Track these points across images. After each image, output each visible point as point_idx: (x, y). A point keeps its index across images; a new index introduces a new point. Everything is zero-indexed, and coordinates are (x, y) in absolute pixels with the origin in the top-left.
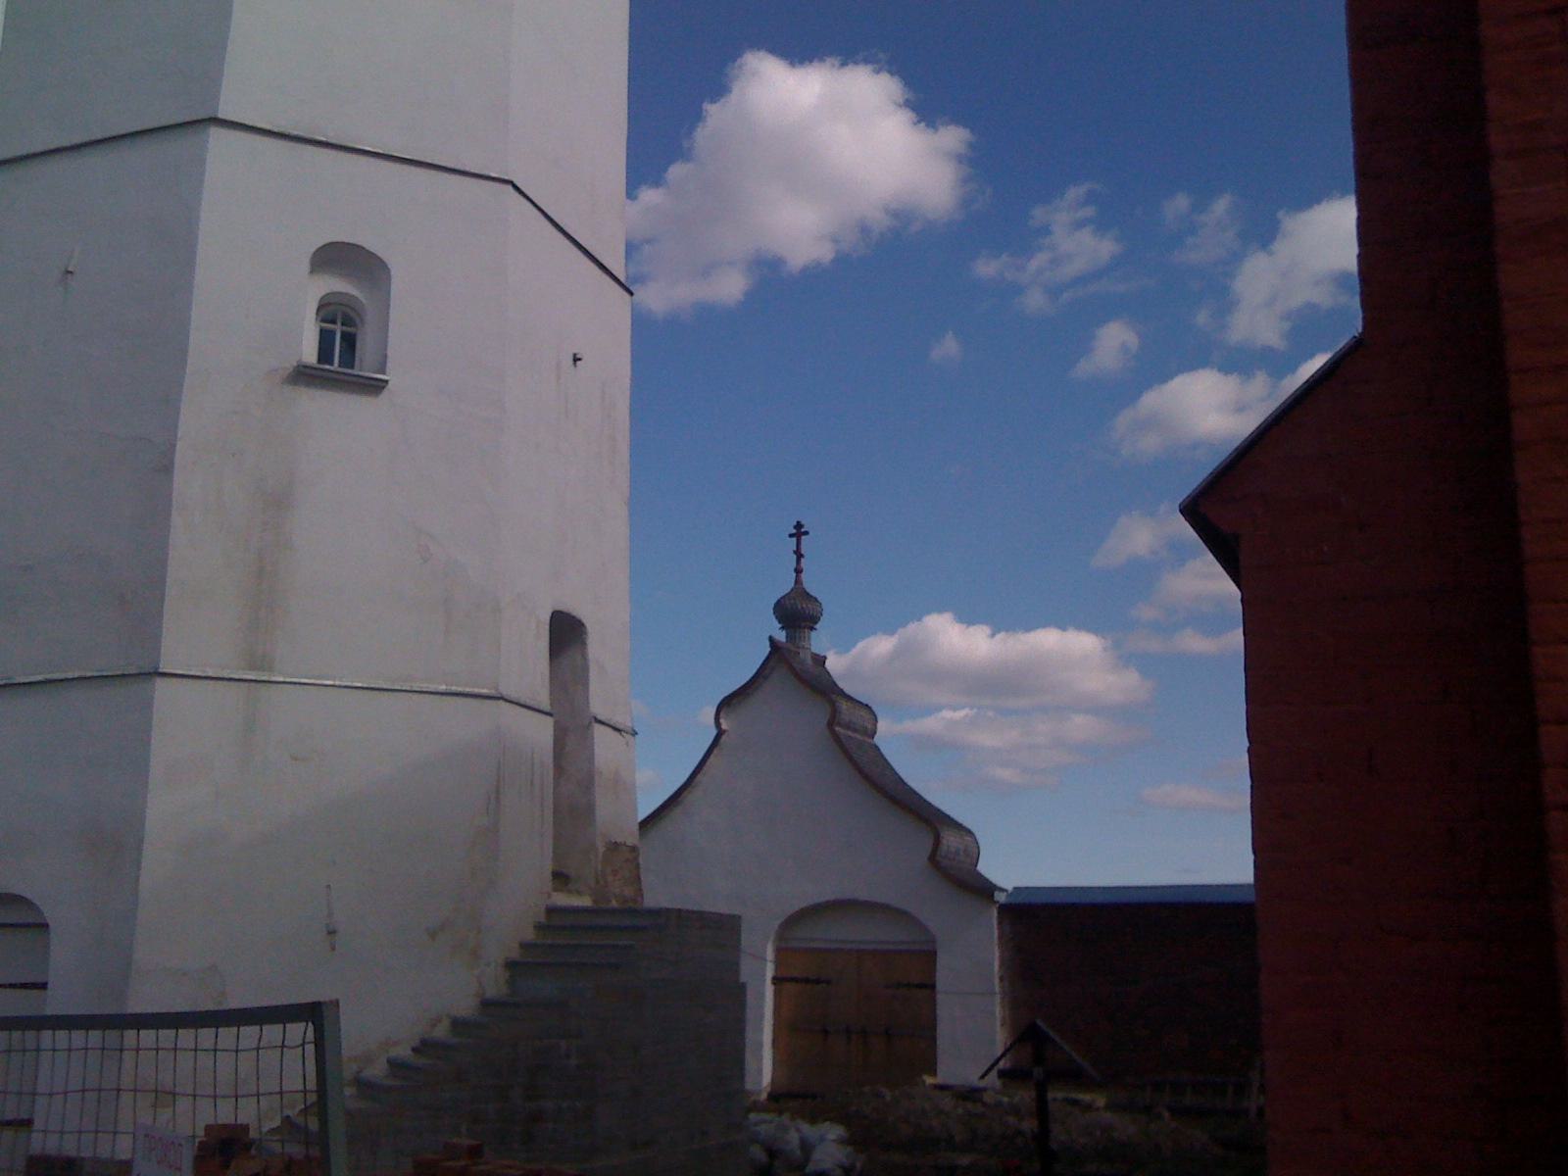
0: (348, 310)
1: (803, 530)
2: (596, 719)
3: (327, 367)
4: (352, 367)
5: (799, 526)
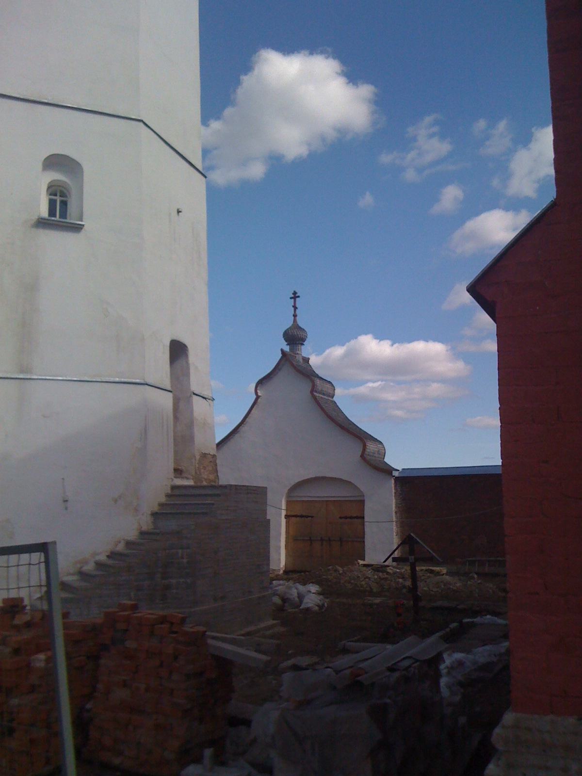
0: (63, 190)
1: (297, 295)
2: (194, 394)
3: (53, 218)
4: (66, 218)
5: (295, 293)
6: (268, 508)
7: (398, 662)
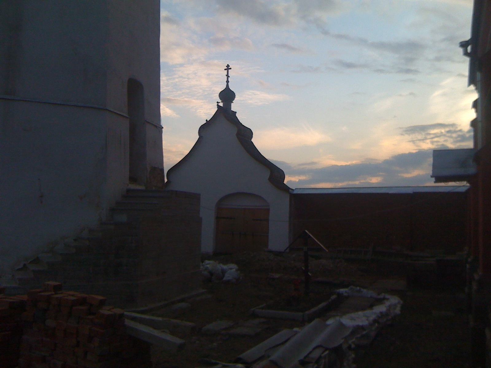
1: (229, 67)
5: (228, 66)
7: (310, 353)
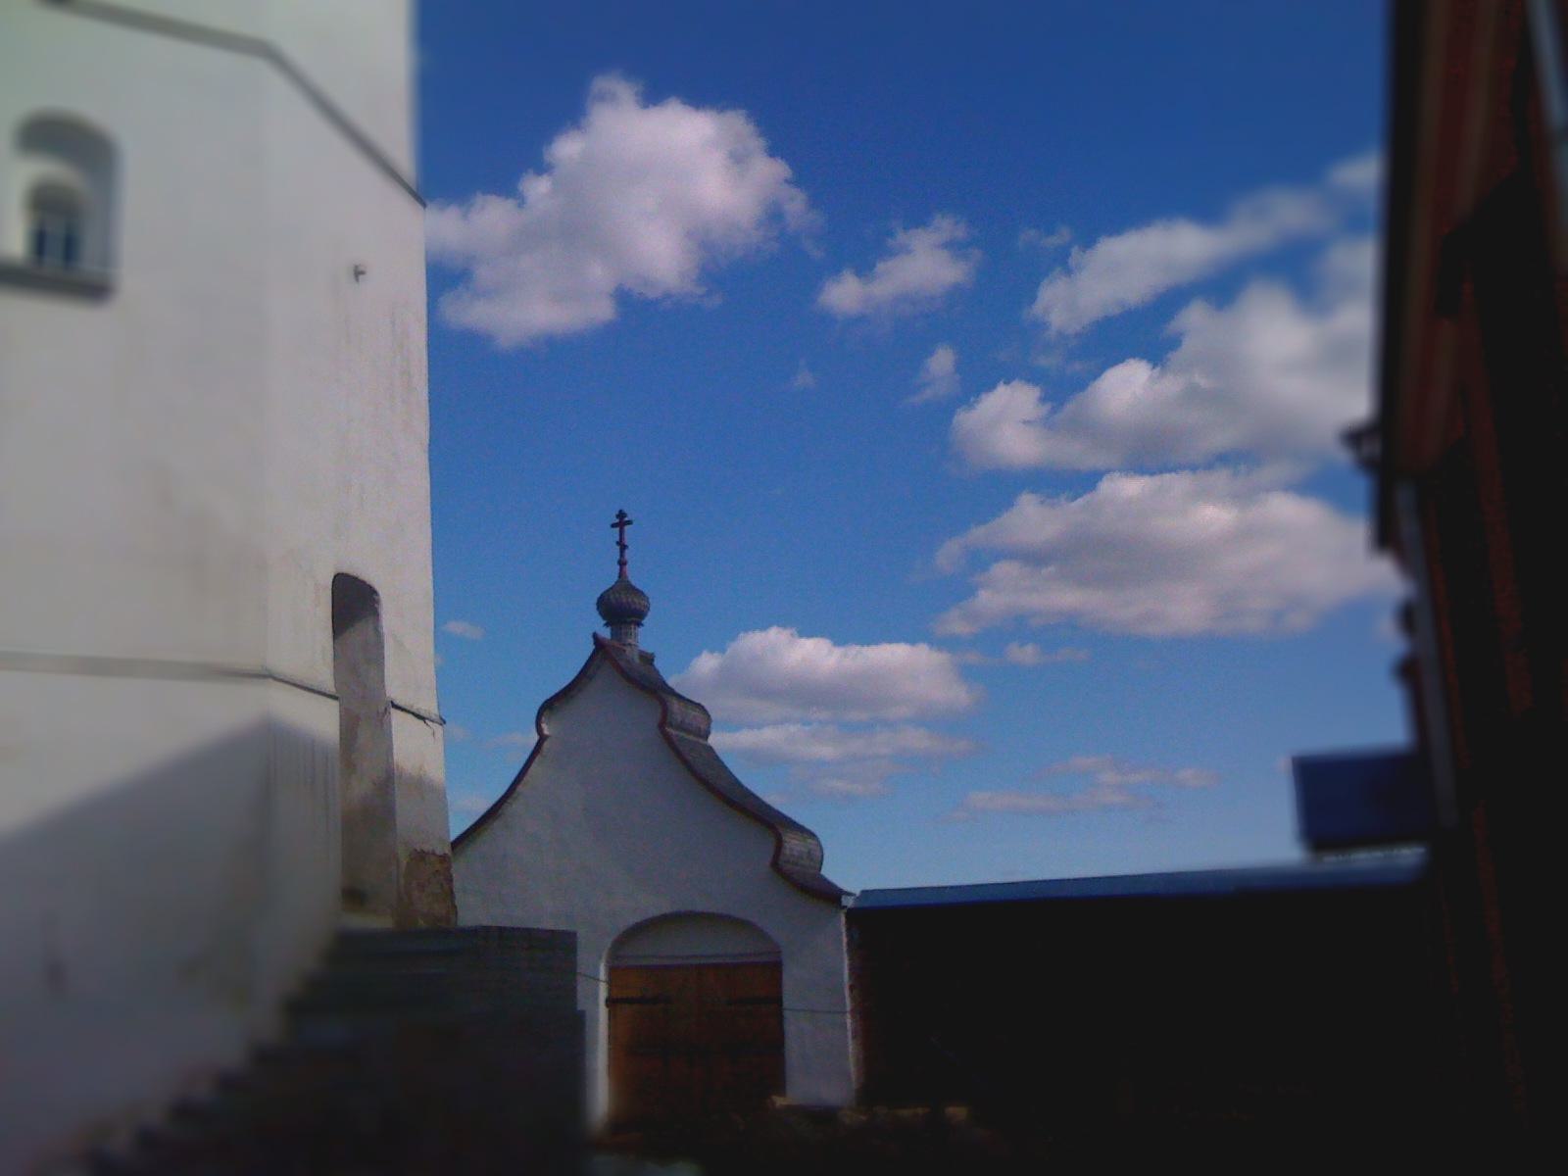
1: (626, 519)
5: (621, 515)
6: (580, 979)
